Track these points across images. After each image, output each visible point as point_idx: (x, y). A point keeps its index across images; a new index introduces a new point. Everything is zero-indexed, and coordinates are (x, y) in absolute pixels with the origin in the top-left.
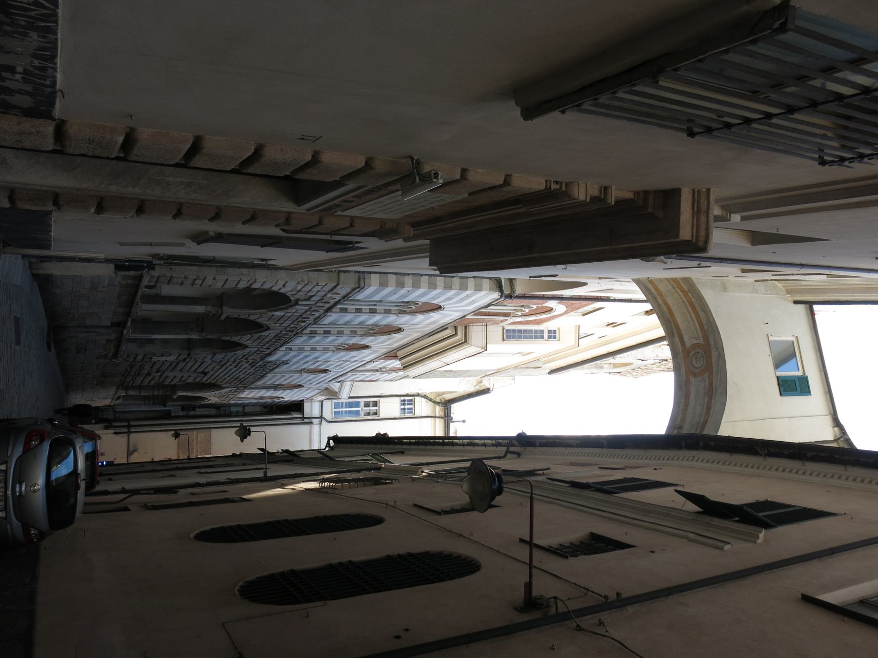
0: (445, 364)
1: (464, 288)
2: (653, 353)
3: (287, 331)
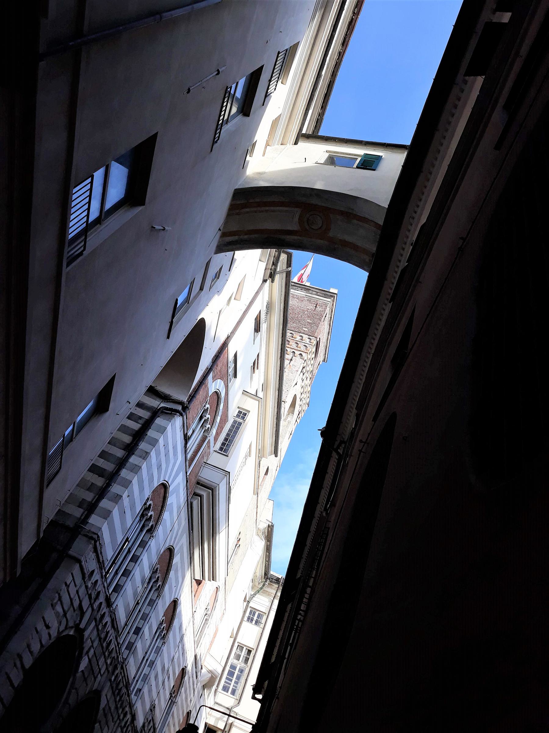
0: (227, 528)
1: (154, 442)
2: (293, 373)
3: (113, 673)
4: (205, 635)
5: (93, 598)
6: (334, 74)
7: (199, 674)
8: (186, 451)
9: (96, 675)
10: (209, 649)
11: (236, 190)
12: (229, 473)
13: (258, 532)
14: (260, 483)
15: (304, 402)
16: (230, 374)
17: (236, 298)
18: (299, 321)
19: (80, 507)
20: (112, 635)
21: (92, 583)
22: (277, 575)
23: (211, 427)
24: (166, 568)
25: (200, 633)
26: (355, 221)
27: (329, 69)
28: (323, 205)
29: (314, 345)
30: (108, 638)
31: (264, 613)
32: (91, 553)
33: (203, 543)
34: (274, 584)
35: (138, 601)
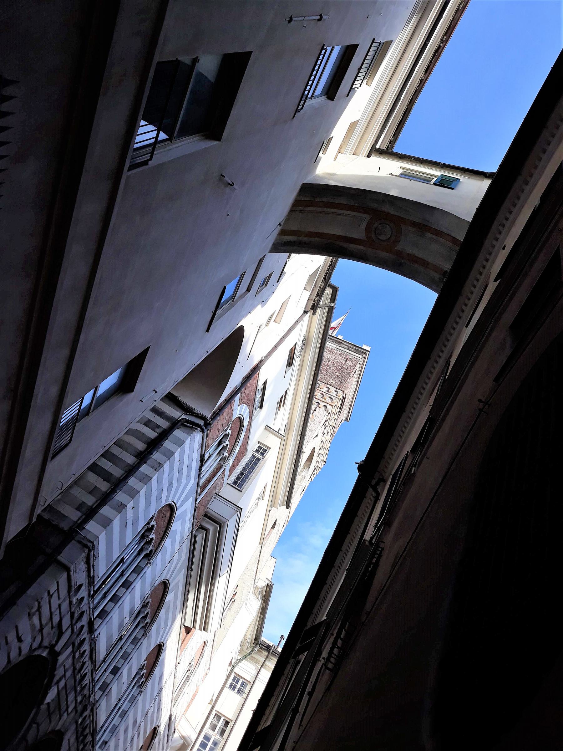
0: (229, 572)
1: (169, 455)
2: (316, 424)
3: (81, 715)
4: (184, 693)
5: (75, 617)
6: (412, 102)
7: (171, 737)
8: (199, 475)
9: (62, 712)
10: (186, 711)
11: (304, 184)
12: (241, 509)
13: (255, 591)
14: (265, 536)
15: (321, 458)
16: (256, 402)
17: (276, 320)
18: (328, 372)
19: (79, 511)
20: (88, 668)
21: (77, 599)
22: (268, 642)
23: (229, 456)
24: (157, 605)
25: (179, 690)
26: (429, 235)
27: (407, 96)
28: (396, 214)
29: (340, 399)
30: (83, 671)
31: (249, 682)
32: (83, 563)
33: (200, 587)
34: (263, 651)
35: (122, 636)
